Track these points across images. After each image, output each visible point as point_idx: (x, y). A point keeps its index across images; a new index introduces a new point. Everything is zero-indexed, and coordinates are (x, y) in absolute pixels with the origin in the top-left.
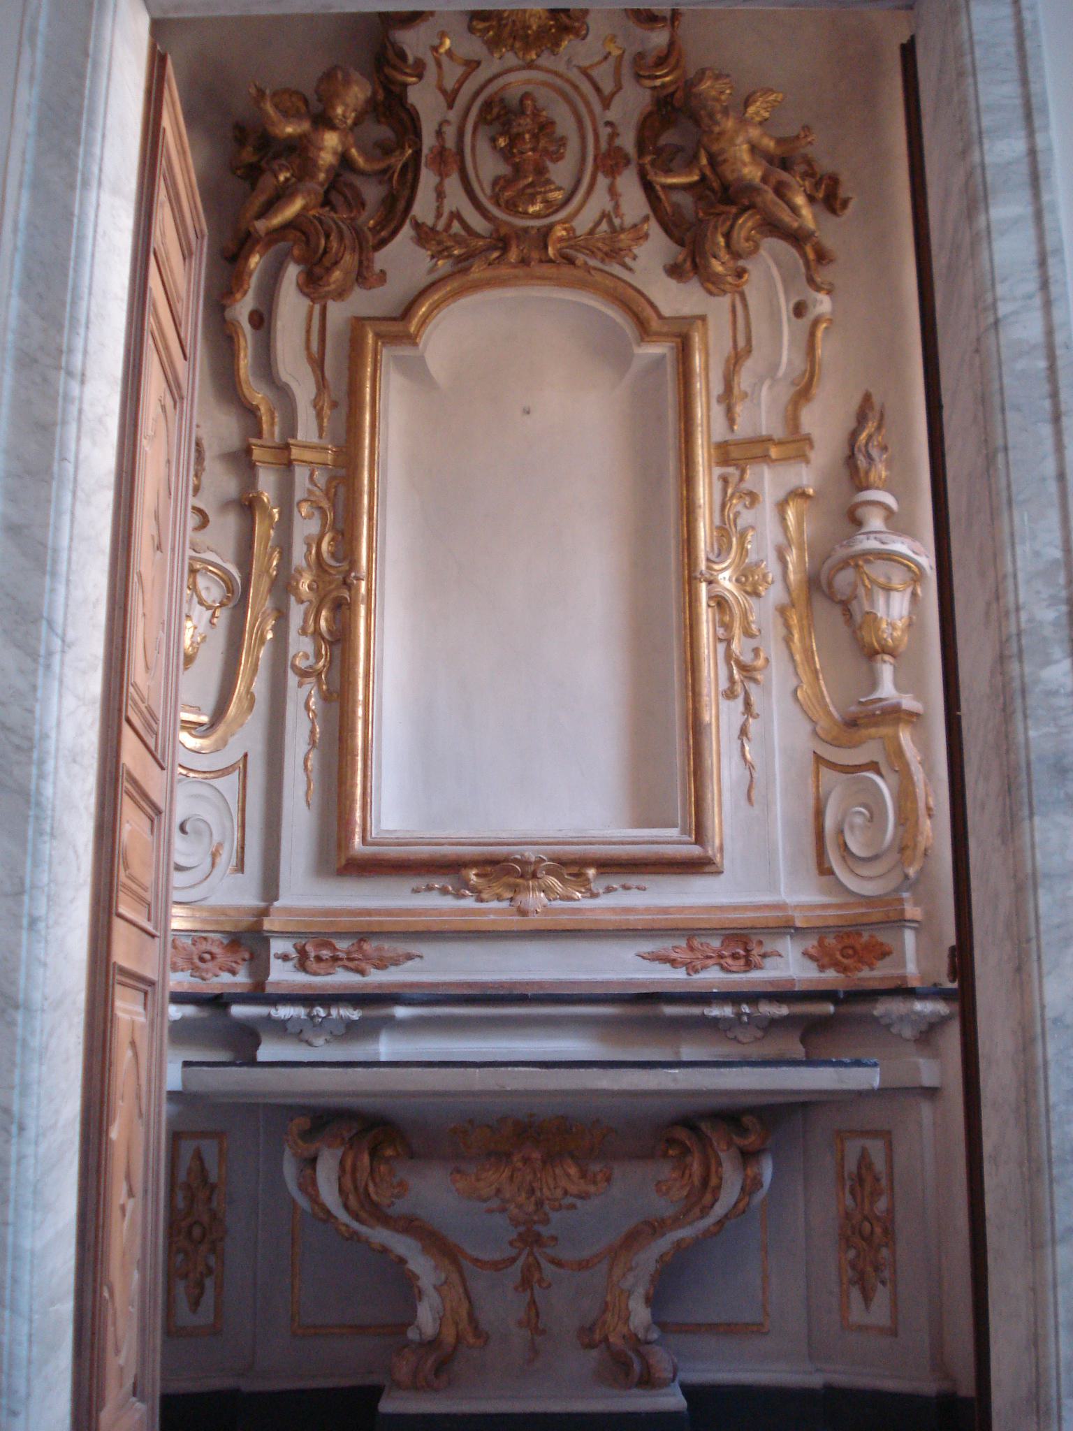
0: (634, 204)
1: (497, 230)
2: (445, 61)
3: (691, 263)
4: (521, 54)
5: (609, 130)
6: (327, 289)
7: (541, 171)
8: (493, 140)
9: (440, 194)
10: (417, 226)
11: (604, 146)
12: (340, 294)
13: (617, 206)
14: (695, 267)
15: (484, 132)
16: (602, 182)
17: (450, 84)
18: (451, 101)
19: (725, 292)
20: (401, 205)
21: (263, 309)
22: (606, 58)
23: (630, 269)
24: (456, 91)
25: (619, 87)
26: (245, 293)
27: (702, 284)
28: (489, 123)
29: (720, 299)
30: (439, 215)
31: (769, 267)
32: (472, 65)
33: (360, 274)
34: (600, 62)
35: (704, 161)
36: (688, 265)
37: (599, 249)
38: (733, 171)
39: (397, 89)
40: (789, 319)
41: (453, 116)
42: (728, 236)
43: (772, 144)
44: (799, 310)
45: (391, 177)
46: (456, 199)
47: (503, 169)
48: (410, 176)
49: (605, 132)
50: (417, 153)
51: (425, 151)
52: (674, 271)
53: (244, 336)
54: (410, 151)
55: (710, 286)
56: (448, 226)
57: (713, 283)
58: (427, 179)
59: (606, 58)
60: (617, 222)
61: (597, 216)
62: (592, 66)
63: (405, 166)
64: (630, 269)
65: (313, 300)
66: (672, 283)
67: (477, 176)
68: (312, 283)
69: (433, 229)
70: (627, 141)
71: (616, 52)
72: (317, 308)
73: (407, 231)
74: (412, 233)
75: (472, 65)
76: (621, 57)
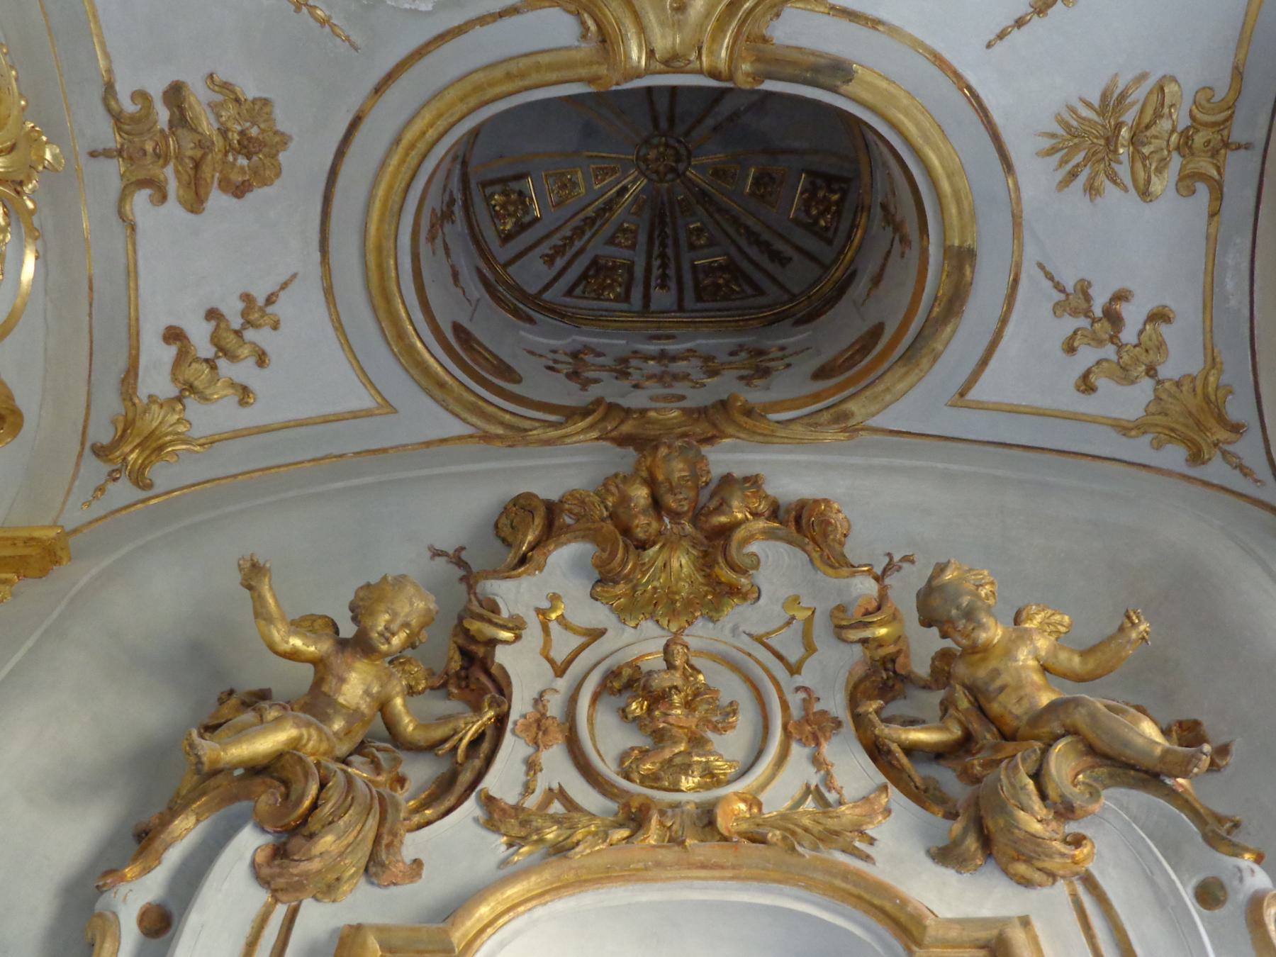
0: (853, 771)
1: (627, 806)
2: (555, 628)
3: (980, 836)
4: (664, 622)
5: (802, 695)
6: (305, 866)
7: (697, 742)
8: (623, 713)
9: (532, 766)
10: (489, 802)
11: (796, 712)
12: (329, 889)
13: (828, 779)
14: (986, 842)
15: (609, 702)
16: (798, 752)
17: (560, 655)
18: (560, 671)
19: (1053, 876)
20: (465, 778)
21: (173, 908)
22: (788, 623)
23: (867, 858)
24: (569, 662)
25: (810, 648)
26: (147, 870)
27: (1005, 871)
28: (613, 692)
29: (1045, 891)
30: (528, 789)
31: (1118, 839)
32: (595, 635)
33: (373, 858)
34: (781, 628)
35: (964, 703)
36: (972, 844)
37: (806, 830)
38: (1020, 699)
39: (481, 651)
40: (1198, 912)
41: (562, 684)
42: (1037, 776)
43: (1076, 660)
44: (1210, 895)
45: (455, 748)
46: (557, 768)
47: (634, 740)
48: (485, 746)
49: (795, 700)
50: (501, 722)
51: (514, 716)
52: (945, 855)
53: (118, 940)
54: (491, 713)
55: (1021, 868)
56: (546, 803)
57: (1028, 861)
58: (512, 750)
59: (788, 623)
60: (831, 797)
61: (797, 791)
62: (768, 634)
63: (476, 743)
64: (867, 858)
65: (274, 892)
66: (949, 874)
67: (598, 752)
68: (279, 869)
69: (517, 808)
70: (835, 704)
71: (802, 615)
72: (281, 911)
73: (470, 807)
74: (478, 812)
75: (595, 635)
76: (809, 622)
